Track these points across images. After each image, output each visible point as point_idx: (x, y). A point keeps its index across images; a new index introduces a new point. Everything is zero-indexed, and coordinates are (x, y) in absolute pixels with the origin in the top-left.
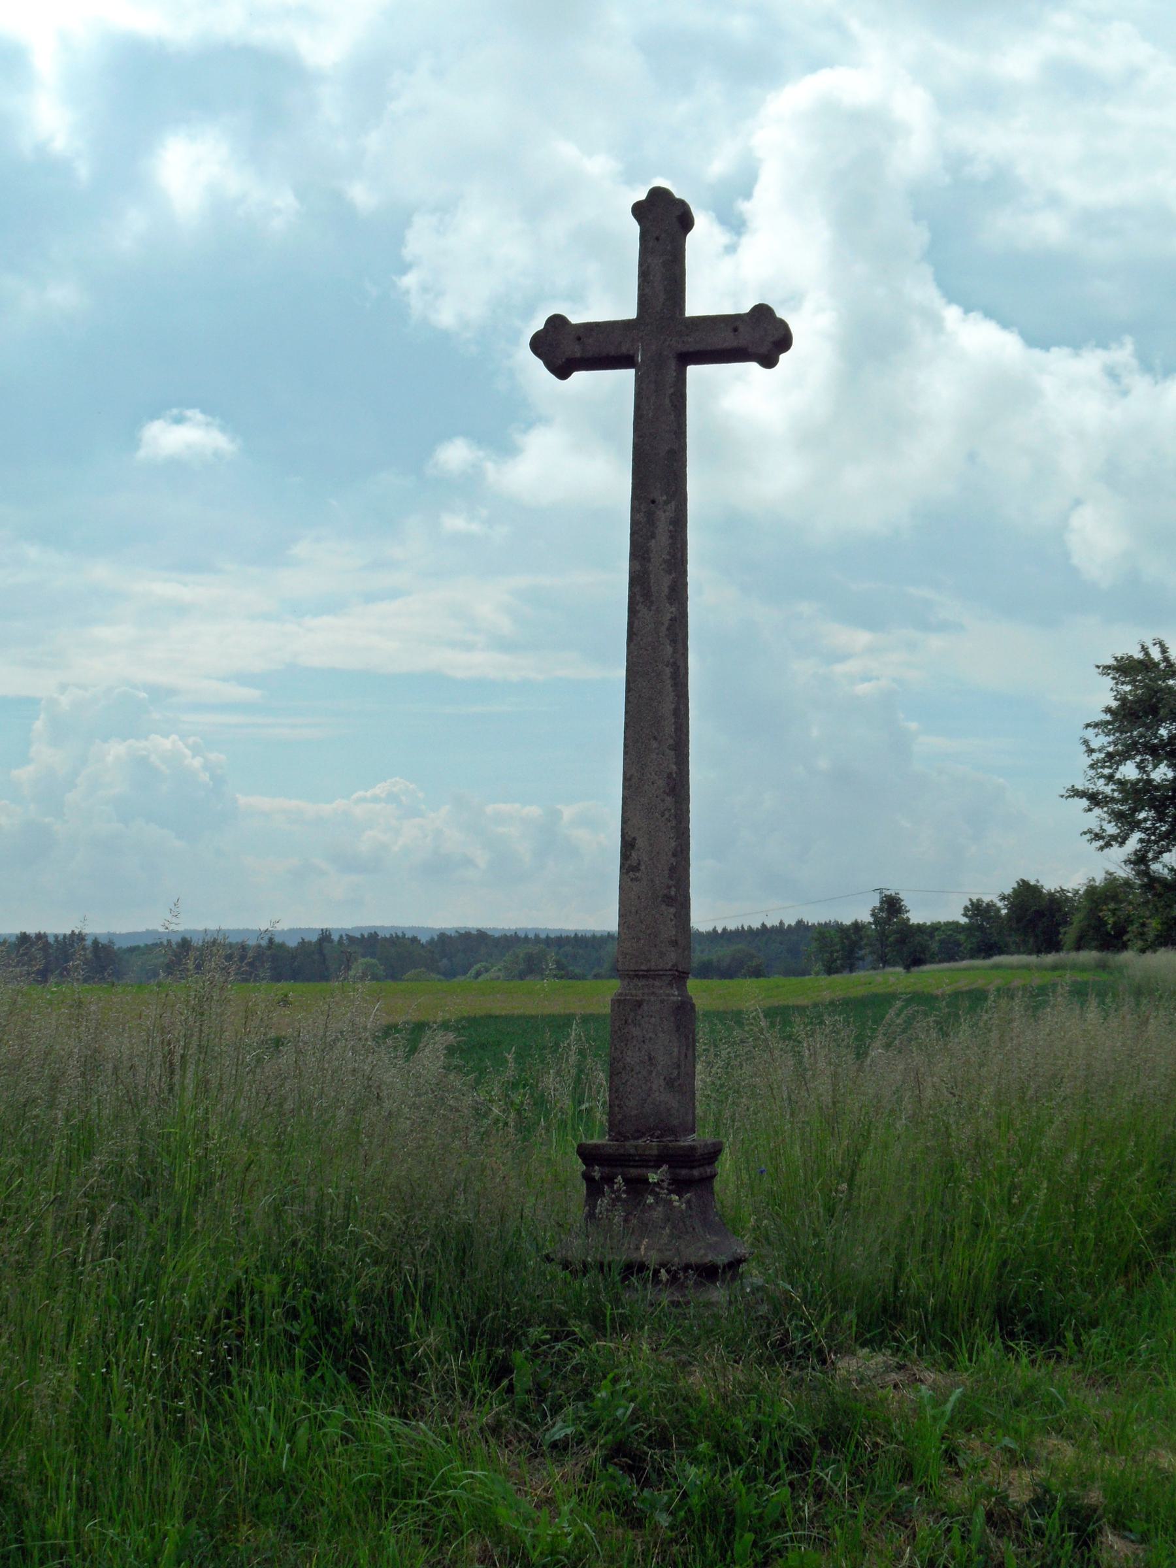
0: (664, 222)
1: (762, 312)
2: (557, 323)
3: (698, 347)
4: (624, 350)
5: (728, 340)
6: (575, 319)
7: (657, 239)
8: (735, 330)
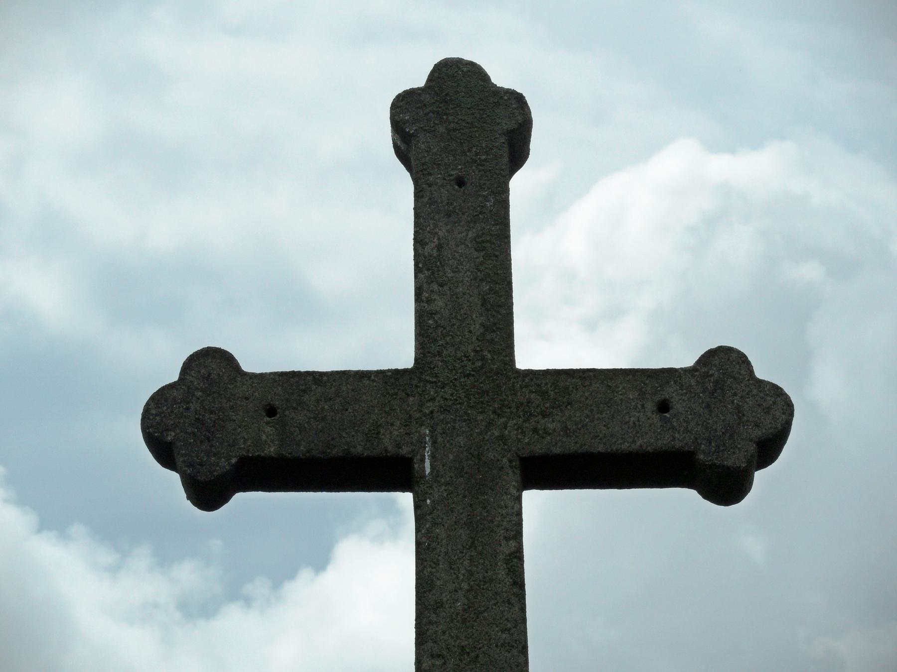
0: (461, 139)
1: (724, 367)
2: (210, 368)
3: (571, 445)
4: (387, 443)
5: (649, 435)
6: (253, 361)
7: (460, 182)
8: (664, 407)
